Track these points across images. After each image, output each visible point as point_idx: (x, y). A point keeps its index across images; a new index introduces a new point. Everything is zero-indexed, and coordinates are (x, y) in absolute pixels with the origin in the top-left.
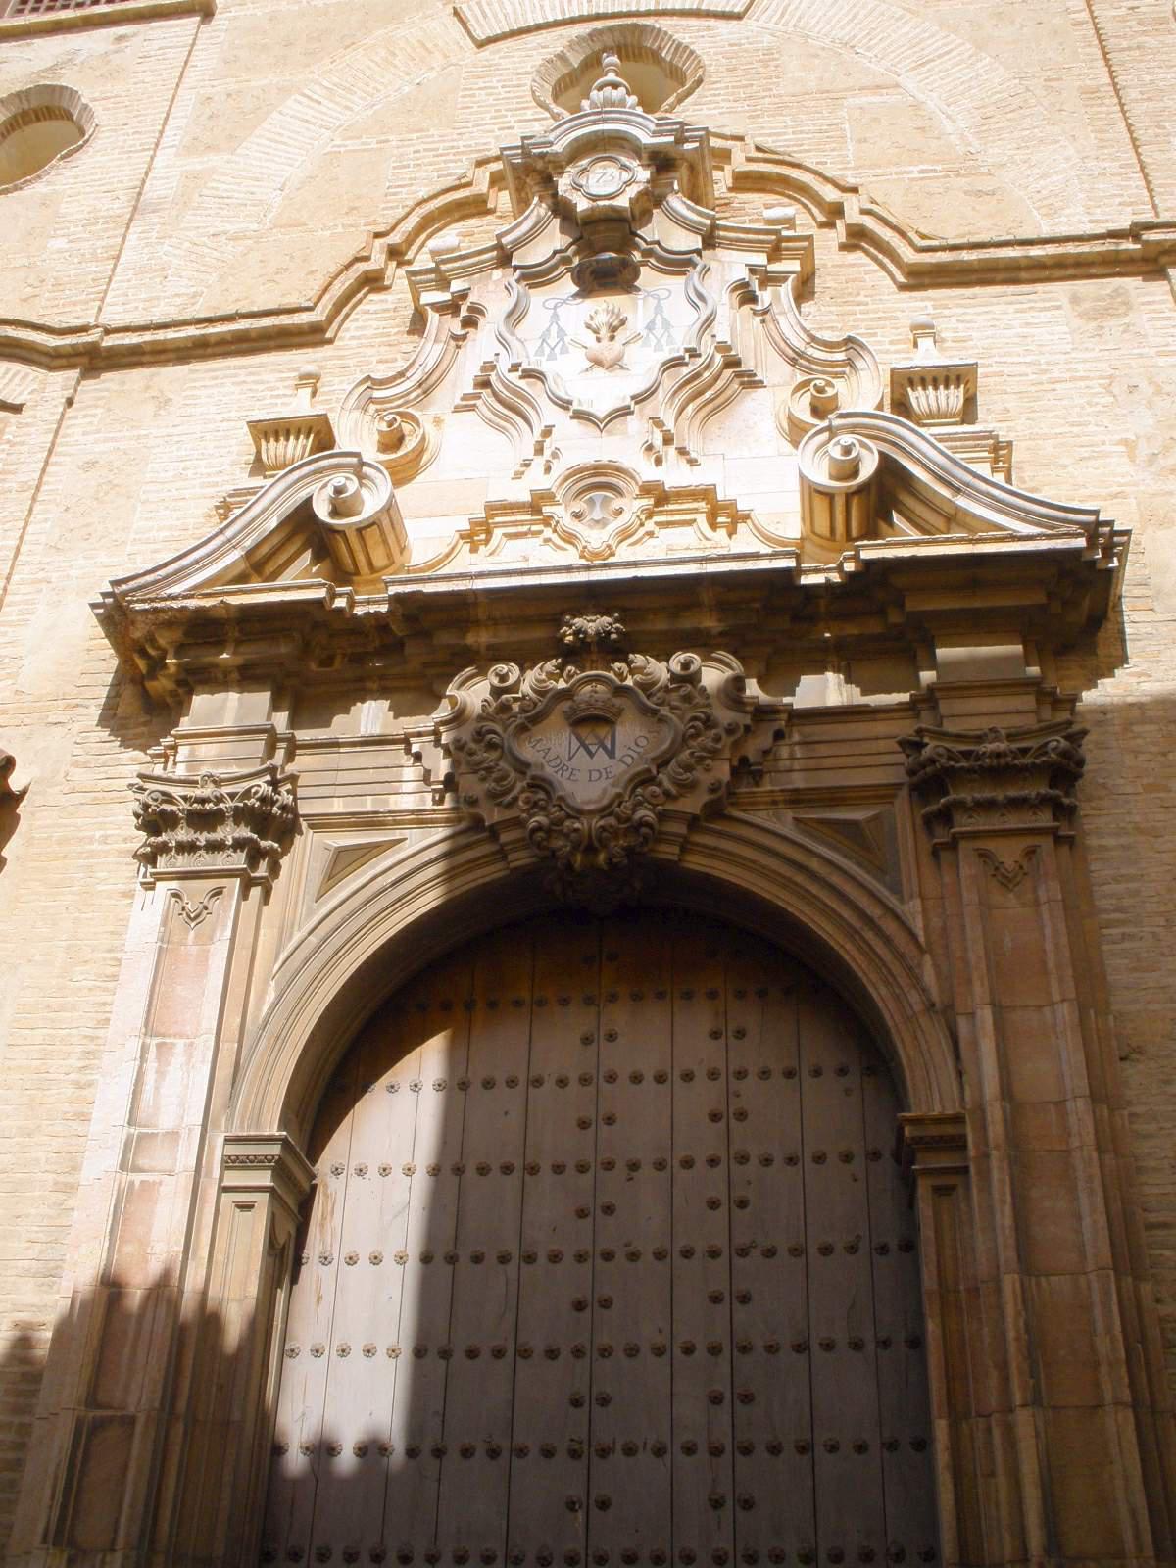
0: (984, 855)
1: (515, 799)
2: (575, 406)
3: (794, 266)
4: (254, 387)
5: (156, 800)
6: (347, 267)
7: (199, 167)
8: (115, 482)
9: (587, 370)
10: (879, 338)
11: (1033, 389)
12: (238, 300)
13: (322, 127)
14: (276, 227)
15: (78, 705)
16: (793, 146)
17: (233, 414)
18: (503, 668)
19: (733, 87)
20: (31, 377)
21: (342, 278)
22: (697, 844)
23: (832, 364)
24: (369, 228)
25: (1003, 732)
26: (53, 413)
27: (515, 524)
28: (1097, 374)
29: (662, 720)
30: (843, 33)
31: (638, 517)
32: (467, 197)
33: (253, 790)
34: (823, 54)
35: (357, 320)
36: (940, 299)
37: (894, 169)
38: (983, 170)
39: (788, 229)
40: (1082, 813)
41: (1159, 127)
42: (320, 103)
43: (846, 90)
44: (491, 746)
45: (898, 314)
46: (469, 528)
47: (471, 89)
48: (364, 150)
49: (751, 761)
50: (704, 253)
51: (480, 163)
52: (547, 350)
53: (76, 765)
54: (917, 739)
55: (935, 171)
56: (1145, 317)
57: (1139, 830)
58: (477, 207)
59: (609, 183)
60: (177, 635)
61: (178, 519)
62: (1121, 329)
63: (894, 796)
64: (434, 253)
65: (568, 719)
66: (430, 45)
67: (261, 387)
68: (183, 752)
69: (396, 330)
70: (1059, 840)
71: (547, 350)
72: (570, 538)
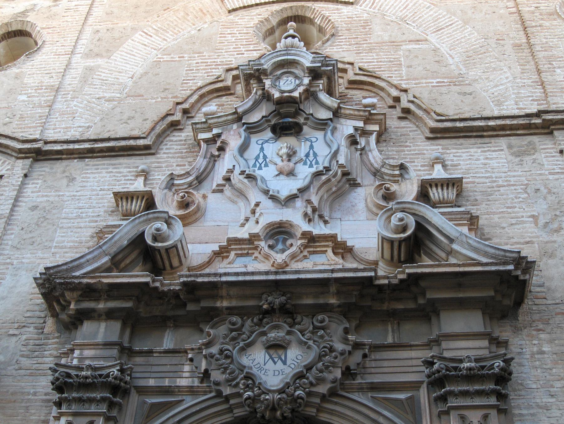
0: (463, 418)
1: (238, 384)
2: (271, 193)
3: (376, 128)
4: (117, 175)
5: (62, 376)
6: (163, 118)
7: (92, 64)
8: (47, 217)
9: (277, 176)
10: (416, 164)
11: (489, 190)
12: (109, 131)
13: (152, 48)
14: (129, 96)
15: (24, 326)
16: (377, 68)
17: (106, 187)
18: (234, 319)
19: (349, 38)
20: (7, 163)
21: (160, 123)
22: (325, 408)
23: (394, 176)
24: (174, 100)
25: (473, 358)
26: (17, 181)
27: (241, 249)
28: (520, 183)
29: (309, 347)
30: (401, 14)
31: (300, 248)
32: (221, 87)
33: (111, 374)
34: (392, 24)
35: (166, 145)
36: (445, 145)
37: (424, 81)
38: (467, 82)
39: (373, 110)
40: (511, 397)
41: (550, 64)
42: (151, 36)
43: (402, 42)
44: (227, 357)
45: (425, 152)
46: (218, 249)
47: (224, 34)
48: (172, 61)
49: (352, 368)
50: (335, 120)
51: (228, 70)
52: (258, 165)
53: (22, 356)
54: (431, 360)
55: (443, 82)
56: (543, 155)
57: (539, 407)
58: (226, 91)
59: (289, 85)
60: (76, 294)
61: (77, 238)
62: (532, 161)
63: (420, 387)
64: (206, 115)
65: (264, 345)
66: (205, 11)
67: (119, 175)
68: (77, 353)
69: (185, 151)
70: (501, 411)
71: (258, 165)
72: (267, 257)
